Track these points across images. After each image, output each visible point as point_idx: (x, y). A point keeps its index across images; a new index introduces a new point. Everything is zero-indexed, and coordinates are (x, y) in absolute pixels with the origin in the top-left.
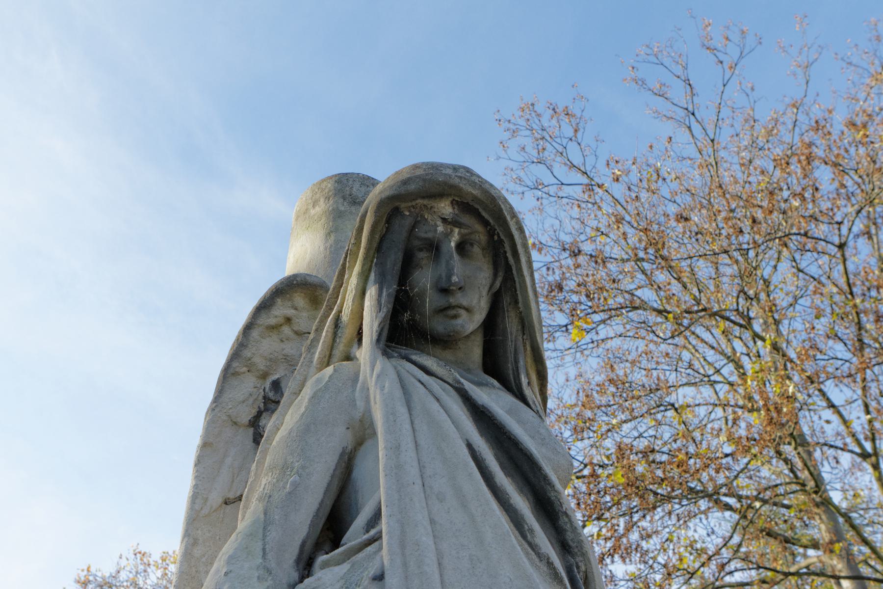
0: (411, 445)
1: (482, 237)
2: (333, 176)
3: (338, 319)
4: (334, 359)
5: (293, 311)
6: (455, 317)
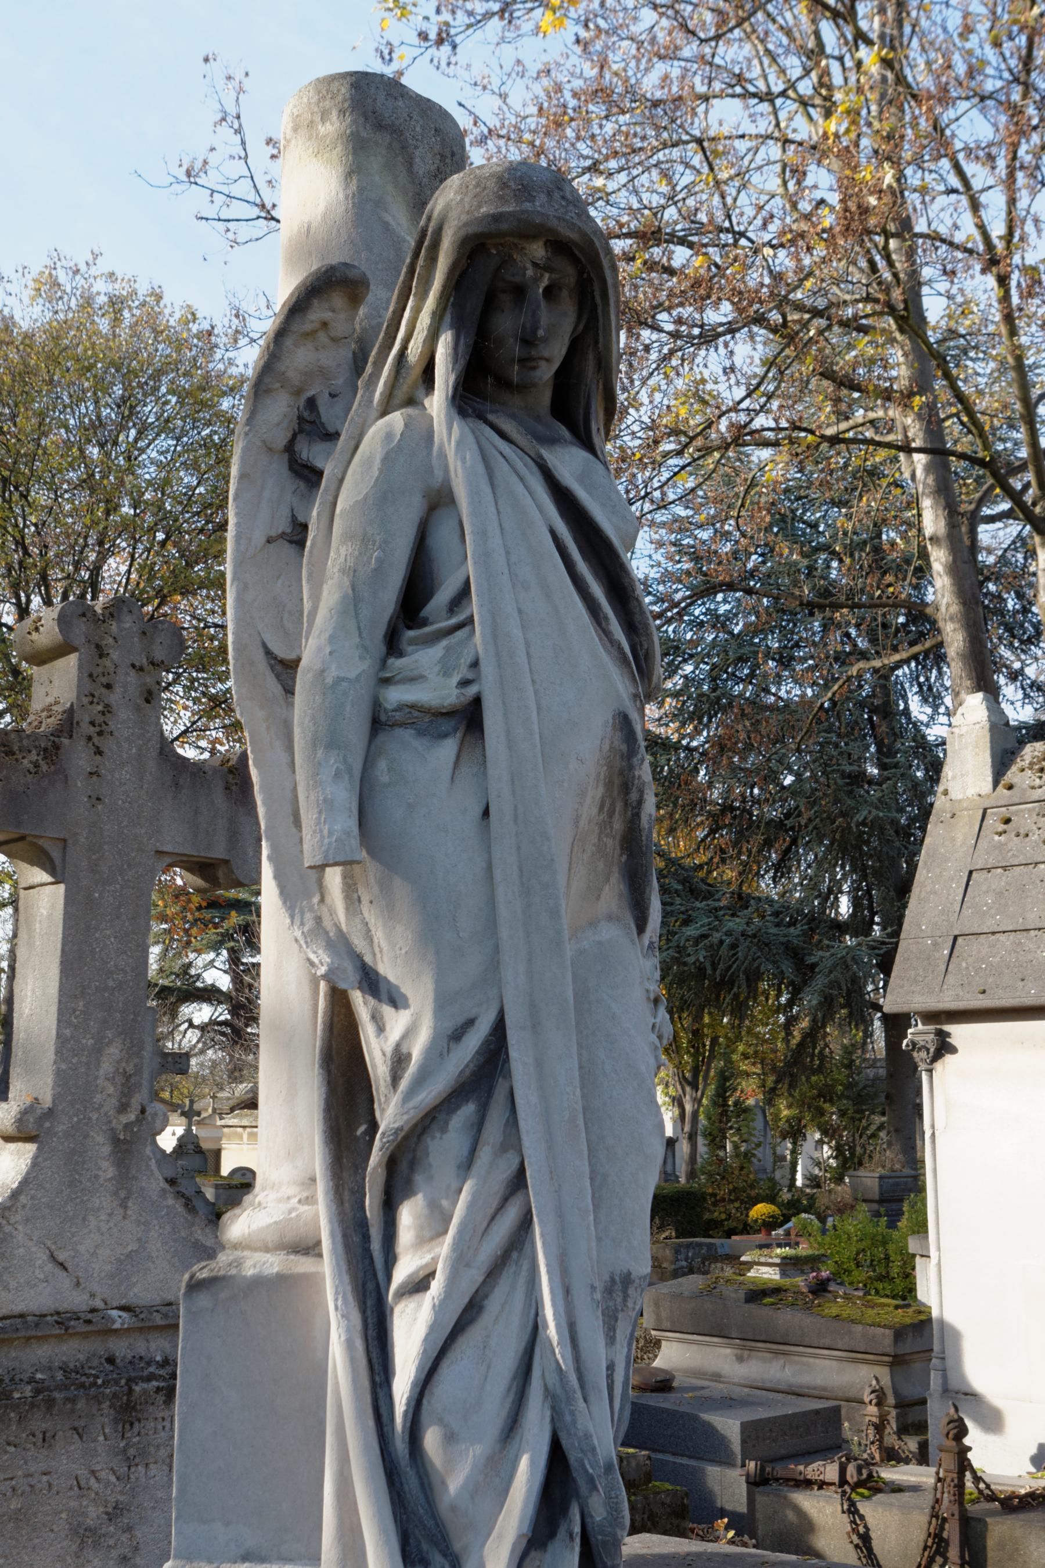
0: (497, 531)
6: (534, 368)
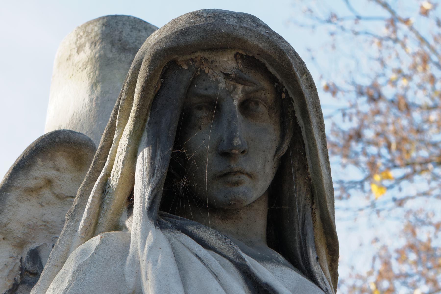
1: (268, 95)
2: (100, 18)
3: (105, 183)
4: (100, 229)
5: (55, 172)
6: (237, 184)
